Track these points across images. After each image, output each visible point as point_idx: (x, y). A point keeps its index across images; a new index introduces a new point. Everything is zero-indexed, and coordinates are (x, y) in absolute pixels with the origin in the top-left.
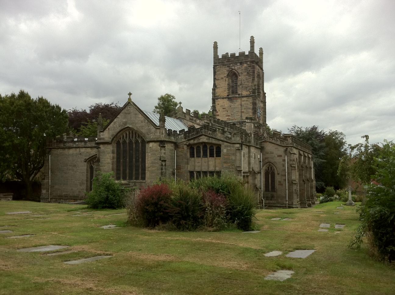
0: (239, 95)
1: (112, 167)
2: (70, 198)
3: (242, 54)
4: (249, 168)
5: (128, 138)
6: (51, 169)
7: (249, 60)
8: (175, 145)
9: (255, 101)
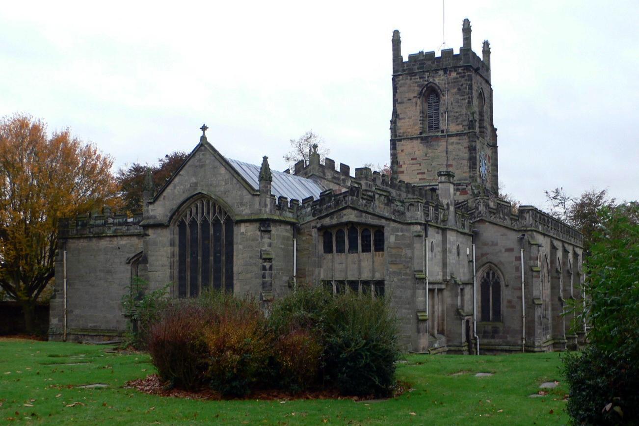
0: (442, 131)
1: (171, 272)
2: (102, 334)
3: (447, 53)
4: (445, 274)
5: (200, 215)
6: (66, 278)
7: (461, 63)
8: (294, 227)
9: (474, 144)
